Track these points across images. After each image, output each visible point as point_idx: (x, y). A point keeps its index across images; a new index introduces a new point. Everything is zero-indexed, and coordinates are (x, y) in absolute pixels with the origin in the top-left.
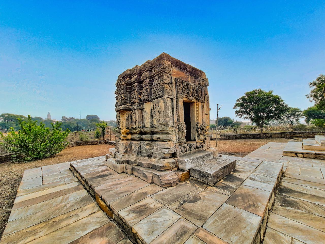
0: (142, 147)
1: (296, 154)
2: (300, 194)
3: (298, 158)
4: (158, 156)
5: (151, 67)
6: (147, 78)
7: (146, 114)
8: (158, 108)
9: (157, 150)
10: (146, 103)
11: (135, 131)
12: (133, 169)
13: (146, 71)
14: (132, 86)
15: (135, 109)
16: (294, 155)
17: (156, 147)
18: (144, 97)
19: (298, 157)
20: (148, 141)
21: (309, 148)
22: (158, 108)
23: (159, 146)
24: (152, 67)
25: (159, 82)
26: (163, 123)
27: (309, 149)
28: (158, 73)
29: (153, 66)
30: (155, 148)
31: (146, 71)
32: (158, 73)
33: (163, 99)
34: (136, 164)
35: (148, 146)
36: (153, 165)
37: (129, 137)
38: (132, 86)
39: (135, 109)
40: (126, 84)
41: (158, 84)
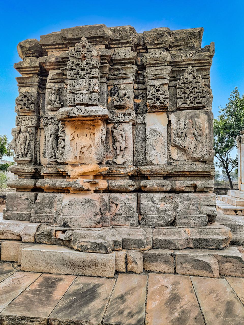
0: (146, 206)
1: (236, 211)
2: (8, 289)
3: (237, 216)
4: (192, 222)
5: (173, 43)
6: (164, 62)
7: (155, 137)
8: (192, 128)
9: (188, 209)
10: (152, 115)
11: (121, 169)
12: (147, 258)
13: (158, 48)
14: (120, 67)
15: (126, 122)
16: (233, 213)
17: (184, 203)
18: (158, 99)
19: (237, 215)
20: (165, 192)
21: (241, 204)
22: (192, 128)
23: (193, 202)
24: (175, 45)
25: (200, 80)
26: (206, 156)
27: (240, 205)
28: (193, 62)
29: (179, 43)
30: (181, 207)
31: (158, 48)
32: (193, 62)
33: (207, 113)
34: (150, 246)
35: (163, 203)
36: (197, 240)
37: (103, 184)
38: (120, 67)
39: (126, 122)
40: (101, 56)
41: (196, 82)
